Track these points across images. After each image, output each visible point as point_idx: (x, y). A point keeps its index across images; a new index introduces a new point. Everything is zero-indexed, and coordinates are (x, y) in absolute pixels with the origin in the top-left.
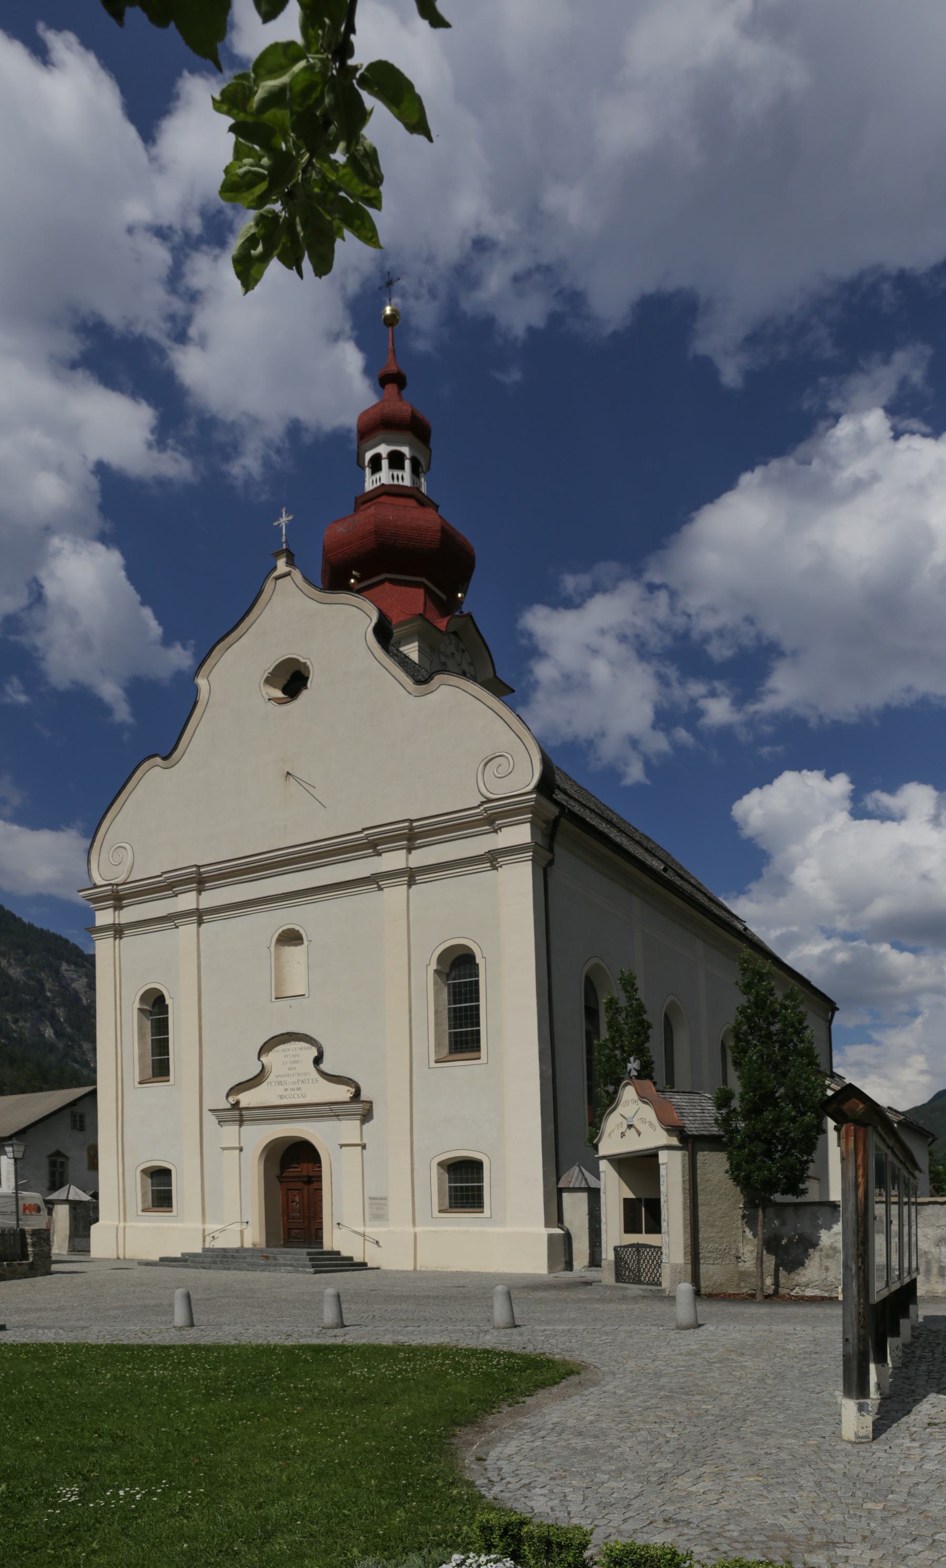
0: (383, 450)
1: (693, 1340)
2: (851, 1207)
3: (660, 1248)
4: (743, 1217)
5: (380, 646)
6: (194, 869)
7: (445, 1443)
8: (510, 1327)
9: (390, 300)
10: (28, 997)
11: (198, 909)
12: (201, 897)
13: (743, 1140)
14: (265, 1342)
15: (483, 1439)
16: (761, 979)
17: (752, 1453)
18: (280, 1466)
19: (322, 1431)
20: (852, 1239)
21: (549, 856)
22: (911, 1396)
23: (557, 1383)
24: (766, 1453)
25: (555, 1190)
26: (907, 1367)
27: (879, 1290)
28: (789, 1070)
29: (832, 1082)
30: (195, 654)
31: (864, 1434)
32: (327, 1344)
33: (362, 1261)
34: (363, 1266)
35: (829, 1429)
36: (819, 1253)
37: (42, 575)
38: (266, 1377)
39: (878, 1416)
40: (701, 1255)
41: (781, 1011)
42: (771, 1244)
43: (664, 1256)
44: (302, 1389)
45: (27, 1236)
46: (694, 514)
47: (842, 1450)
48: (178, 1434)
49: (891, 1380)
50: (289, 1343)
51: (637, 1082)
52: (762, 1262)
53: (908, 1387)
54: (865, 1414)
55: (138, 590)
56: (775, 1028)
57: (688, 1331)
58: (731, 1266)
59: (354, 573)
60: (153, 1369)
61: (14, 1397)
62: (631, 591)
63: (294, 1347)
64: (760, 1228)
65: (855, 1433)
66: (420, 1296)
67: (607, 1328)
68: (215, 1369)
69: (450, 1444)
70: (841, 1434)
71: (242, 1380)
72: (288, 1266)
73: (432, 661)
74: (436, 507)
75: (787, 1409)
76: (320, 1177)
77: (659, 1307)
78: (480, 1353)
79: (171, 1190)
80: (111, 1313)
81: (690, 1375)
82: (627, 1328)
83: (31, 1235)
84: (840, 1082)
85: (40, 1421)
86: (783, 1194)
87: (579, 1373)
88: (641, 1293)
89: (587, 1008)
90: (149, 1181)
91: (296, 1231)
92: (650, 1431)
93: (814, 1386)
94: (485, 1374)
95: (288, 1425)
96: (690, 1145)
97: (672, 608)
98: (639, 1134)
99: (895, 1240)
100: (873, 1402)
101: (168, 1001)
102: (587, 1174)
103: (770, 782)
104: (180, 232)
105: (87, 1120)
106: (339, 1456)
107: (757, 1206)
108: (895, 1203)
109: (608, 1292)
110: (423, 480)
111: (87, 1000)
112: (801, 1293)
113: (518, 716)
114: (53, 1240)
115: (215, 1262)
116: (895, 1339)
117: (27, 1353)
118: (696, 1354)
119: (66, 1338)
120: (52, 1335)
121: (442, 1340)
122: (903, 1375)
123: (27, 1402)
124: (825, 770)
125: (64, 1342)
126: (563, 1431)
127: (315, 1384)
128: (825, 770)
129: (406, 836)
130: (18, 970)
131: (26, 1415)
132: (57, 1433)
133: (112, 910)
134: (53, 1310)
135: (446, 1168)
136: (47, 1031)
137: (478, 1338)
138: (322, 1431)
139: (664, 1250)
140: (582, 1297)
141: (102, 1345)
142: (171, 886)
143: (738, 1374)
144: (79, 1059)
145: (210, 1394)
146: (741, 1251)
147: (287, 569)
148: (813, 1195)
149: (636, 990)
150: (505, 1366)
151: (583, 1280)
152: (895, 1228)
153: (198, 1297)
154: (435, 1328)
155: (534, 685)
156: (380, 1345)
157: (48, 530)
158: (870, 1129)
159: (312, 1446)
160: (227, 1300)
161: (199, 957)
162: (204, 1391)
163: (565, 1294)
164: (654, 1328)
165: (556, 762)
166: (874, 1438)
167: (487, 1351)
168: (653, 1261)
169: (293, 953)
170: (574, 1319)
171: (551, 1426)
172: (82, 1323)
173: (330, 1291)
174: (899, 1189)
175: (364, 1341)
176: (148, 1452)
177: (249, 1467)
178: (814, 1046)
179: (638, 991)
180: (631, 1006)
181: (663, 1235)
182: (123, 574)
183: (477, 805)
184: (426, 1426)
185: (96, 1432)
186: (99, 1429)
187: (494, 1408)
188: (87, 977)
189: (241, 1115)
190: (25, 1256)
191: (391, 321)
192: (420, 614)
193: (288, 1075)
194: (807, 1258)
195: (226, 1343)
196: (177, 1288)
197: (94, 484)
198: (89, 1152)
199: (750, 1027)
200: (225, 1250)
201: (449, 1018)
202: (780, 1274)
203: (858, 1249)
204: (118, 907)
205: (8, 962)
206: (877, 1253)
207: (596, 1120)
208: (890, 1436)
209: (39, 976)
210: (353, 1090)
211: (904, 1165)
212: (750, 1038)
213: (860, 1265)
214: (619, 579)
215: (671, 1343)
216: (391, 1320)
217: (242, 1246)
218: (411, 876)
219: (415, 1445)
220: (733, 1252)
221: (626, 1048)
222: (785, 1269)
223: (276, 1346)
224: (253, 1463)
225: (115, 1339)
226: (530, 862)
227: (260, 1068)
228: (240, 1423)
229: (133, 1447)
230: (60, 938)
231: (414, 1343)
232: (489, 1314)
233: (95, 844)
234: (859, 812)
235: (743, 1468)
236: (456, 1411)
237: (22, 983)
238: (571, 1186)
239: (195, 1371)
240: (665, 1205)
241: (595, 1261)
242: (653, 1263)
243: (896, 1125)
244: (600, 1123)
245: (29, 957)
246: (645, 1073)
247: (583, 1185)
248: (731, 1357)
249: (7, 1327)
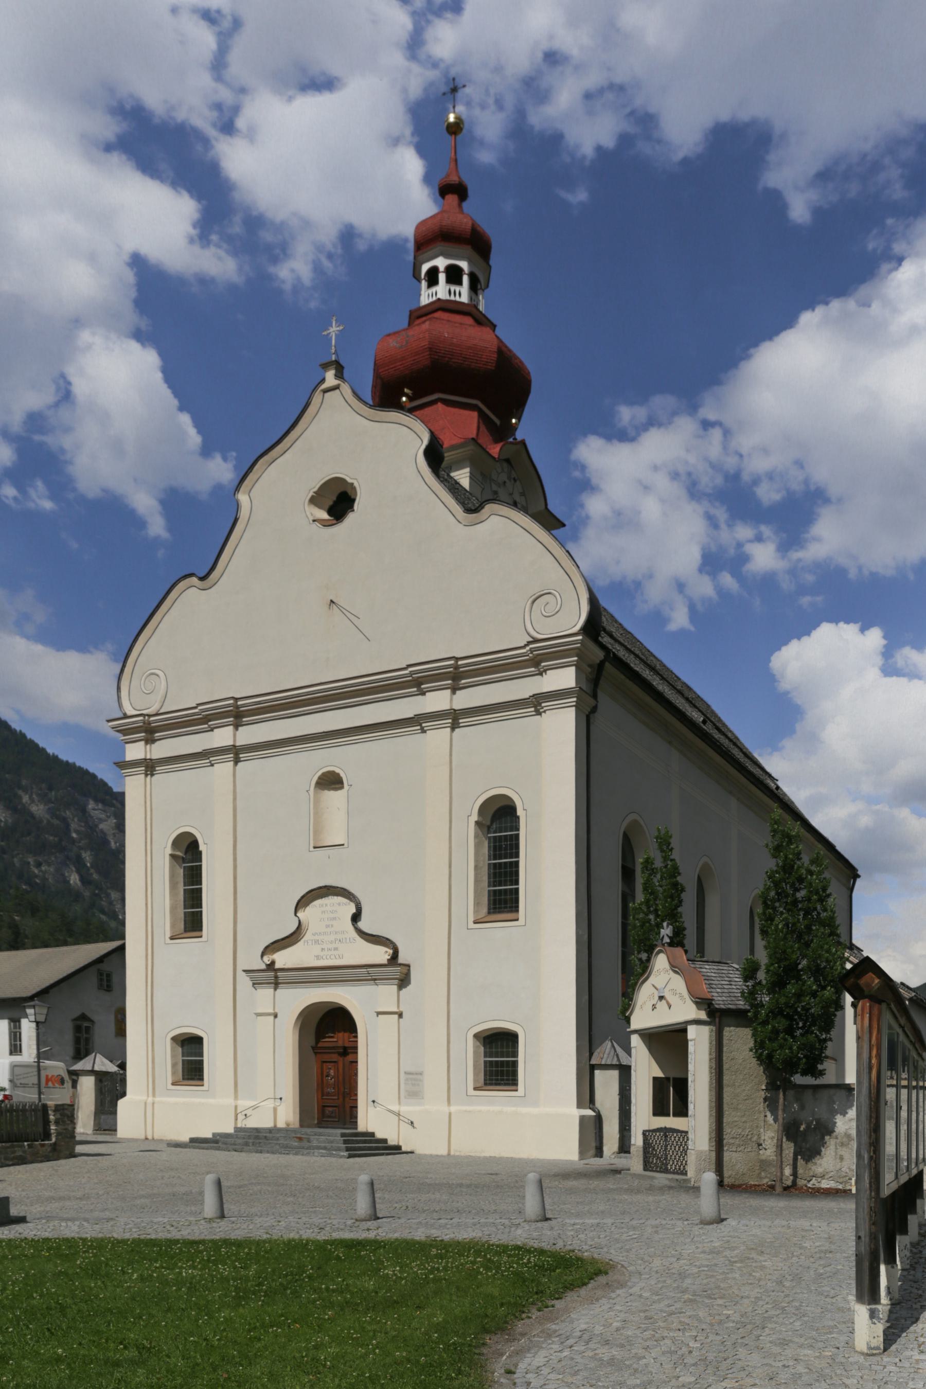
0: (441, 263)
1: (716, 1235)
2: (865, 1090)
3: (686, 1132)
4: (765, 1099)
5: (430, 470)
6: (231, 702)
7: (475, 1353)
8: (541, 1221)
9: (454, 107)
10: (51, 838)
11: (234, 746)
12: (238, 733)
13: (767, 1015)
14: (297, 1237)
15: (512, 1348)
16: (790, 842)
17: (771, 1365)
18: (310, 1381)
19: (353, 1339)
20: (865, 1126)
21: (592, 702)
22: (919, 1302)
23: (585, 1284)
24: (784, 1366)
25: (588, 1067)
26: (914, 1269)
27: (890, 1183)
28: (812, 941)
29: (851, 955)
30: (236, 468)
31: (876, 1345)
32: (360, 1238)
33: (396, 1144)
34: (397, 1149)
35: (843, 1338)
36: (835, 1140)
37: (71, 371)
38: (297, 1277)
39: (888, 1325)
40: (725, 1142)
41: (806, 877)
42: (791, 1131)
43: (690, 1142)
44: (333, 1291)
45: (50, 1112)
46: (752, 351)
47: (855, 1363)
48: (207, 1344)
49: (900, 1283)
50: (322, 1237)
51: (668, 949)
52: (781, 1150)
53: (916, 1291)
54: (876, 1322)
55: (176, 394)
56: (801, 894)
57: (711, 1226)
58: (753, 1154)
59: (406, 390)
60: (181, 1268)
61: (35, 1302)
62: (686, 426)
63: (326, 1242)
64: (780, 1112)
65: (867, 1344)
66: (453, 1184)
67: (634, 1222)
68: (245, 1268)
69: (479, 1354)
70: (854, 1344)
71: (273, 1280)
72: (322, 1149)
73: (483, 489)
74: (493, 327)
75: (804, 1316)
76: (356, 1048)
77: (685, 1199)
78: (511, 1250)
79: (202, 1061)
80: (138, 1202)
81: (712, 1276)
82: (654, 1222)
83: (54, 1111)
84: (858, 955)
85: (63, 1330)
86: (802, 1075)
87: (606, 1273)
88: (667, 1183)
89: (624, 868)
90: (180, 1049)
91: (330, 1109)
92: (674, 1340)
93: (828, 1289)
94: (517, 1274)
95: (319, 1332)
96: (717, 1020)
97: (725, 447)
98: (670, 1007)
99: (904, 1128)
100: (884, 1308)
101: (202, 847)
102: (619, 1049)
103: (808, 633)
104: (229, 18)
105: (115, 979)
106: (370, 1369)
107: (777, 1088)
108: (904, 1087)
109: (636, 1182)
110: (481, 297)
111: (116, 843)
112: (817, 1185)
113: (568, 552)
114: (78, 1117)
115: (247, 1144)
116: (904, 1237)
117: (49, 1249)
118: (718, 1253)
119: (91, 1231)
120: (75, 1228)
121: (474, 1234)
122: (911, 1277)
123: (49, 1308)
124: (860, 623)
125: (88, 1236)
126: (590, 1339)
127: (347, 1285)
128: (860, 623)
129: (452, 674)
130: (42, 807)
131: (48, 1323)
132: (80, 1344)
133: (143, 743)
134: (77, 1199)
135: (482, 1040)
136: (72, 877)
137: (509, 1232)
138: (353, 1339)
139: (690, 1136)
140: (611, 1187)
141: (128, 1240)
142: (206, 719)
143: (757, 1275)
144: (106, 909)
145: (240, 1297)
146: (763, 1138)
147: (335, 382)
148: (830, 1078)
149: (671, 850)
150: (536, 1265)
151: (613, 1167)
152: (904, 1114)
153: (229, 1184)
154: (468, 1220)
155: (585, 520)
156: (412, 1240)
157: (78, 322)
158: (884, 1006)
159: (343, 1357)
160: (259, 1187)
161: (235, 799)
162: (233, 1294)
163: (595, 1183)
164: (679, 1223)
165: (604, 602)
166: (885, 1350)
167: (518, 1248)
168: (679, 1147)
169: (333, 797)
170: (603, 1212)
171: (579, 1334)
172: (107, 1214)
173: (364, 1178)
174: (908, 1071)
175: (396, 1235)
176: (176, 1365)
177: (278, 1383)
178: (836, 915)
179: (673, 851)
180: (666, 867)
181: (689, 1118)
182: (159, 375)
183: (522, 644)
184: (456, 1334)
185: (121, 1343)
186: (124, 1339)
187: (524, 1312)
188: (116, 817)
189: (276, 977)
190: (47, 1136)
191: (455, 129)
192: (473, 439)
193: (325, 933)
194: (823, 1146)
195: (258, 1238)
196: (208, 1173)
197: (130, 276)
198: (116, 1017)
199: (777, 893)
200: (257, 1130)
201: (489, 874)
202: (799, 1164)
203: (870, 1137)
204: (150, 741)
205: (30, 797)
206: (887, 1141)
207: (629, 990)
208: (900, 1347)
209: (63, 814)
210: (391, 951)
211: (913, 1044)
212: (777, 904)
213: (872, 1154)
214: (674, 414)
215: (695, 1239)
216: (424, 1211)
217: (275, 1126)
218: (455, 718)
219: (445, 1356)
220: (755, 1139)
221: (660, 913)
222: (803, 1158)
223: (307, 1241)
224: (283, 1378)
225: (142, 1232)
226: (574, 708)
227: (296, 925)
228: (270, 1330)
229: (159, 1360)
230: (86, 772)
231: (446, 1238)
232: (520, 1205)
233: (126, 670)
234: (890, 670)
235: (762, 1383)
236: (487, 1316)
237: (45, 822)
238: (603, 1063)
239: (224, 1270)
240: (693, 1086)
241: (624, 1147)
242: (679, 1149)
243: (907, 1002)
244: (633, 994)
245: (53, 793)
246: (677, 940)
247: (615, 1062)
248: (751, 1256)
249: (28, 1219)
